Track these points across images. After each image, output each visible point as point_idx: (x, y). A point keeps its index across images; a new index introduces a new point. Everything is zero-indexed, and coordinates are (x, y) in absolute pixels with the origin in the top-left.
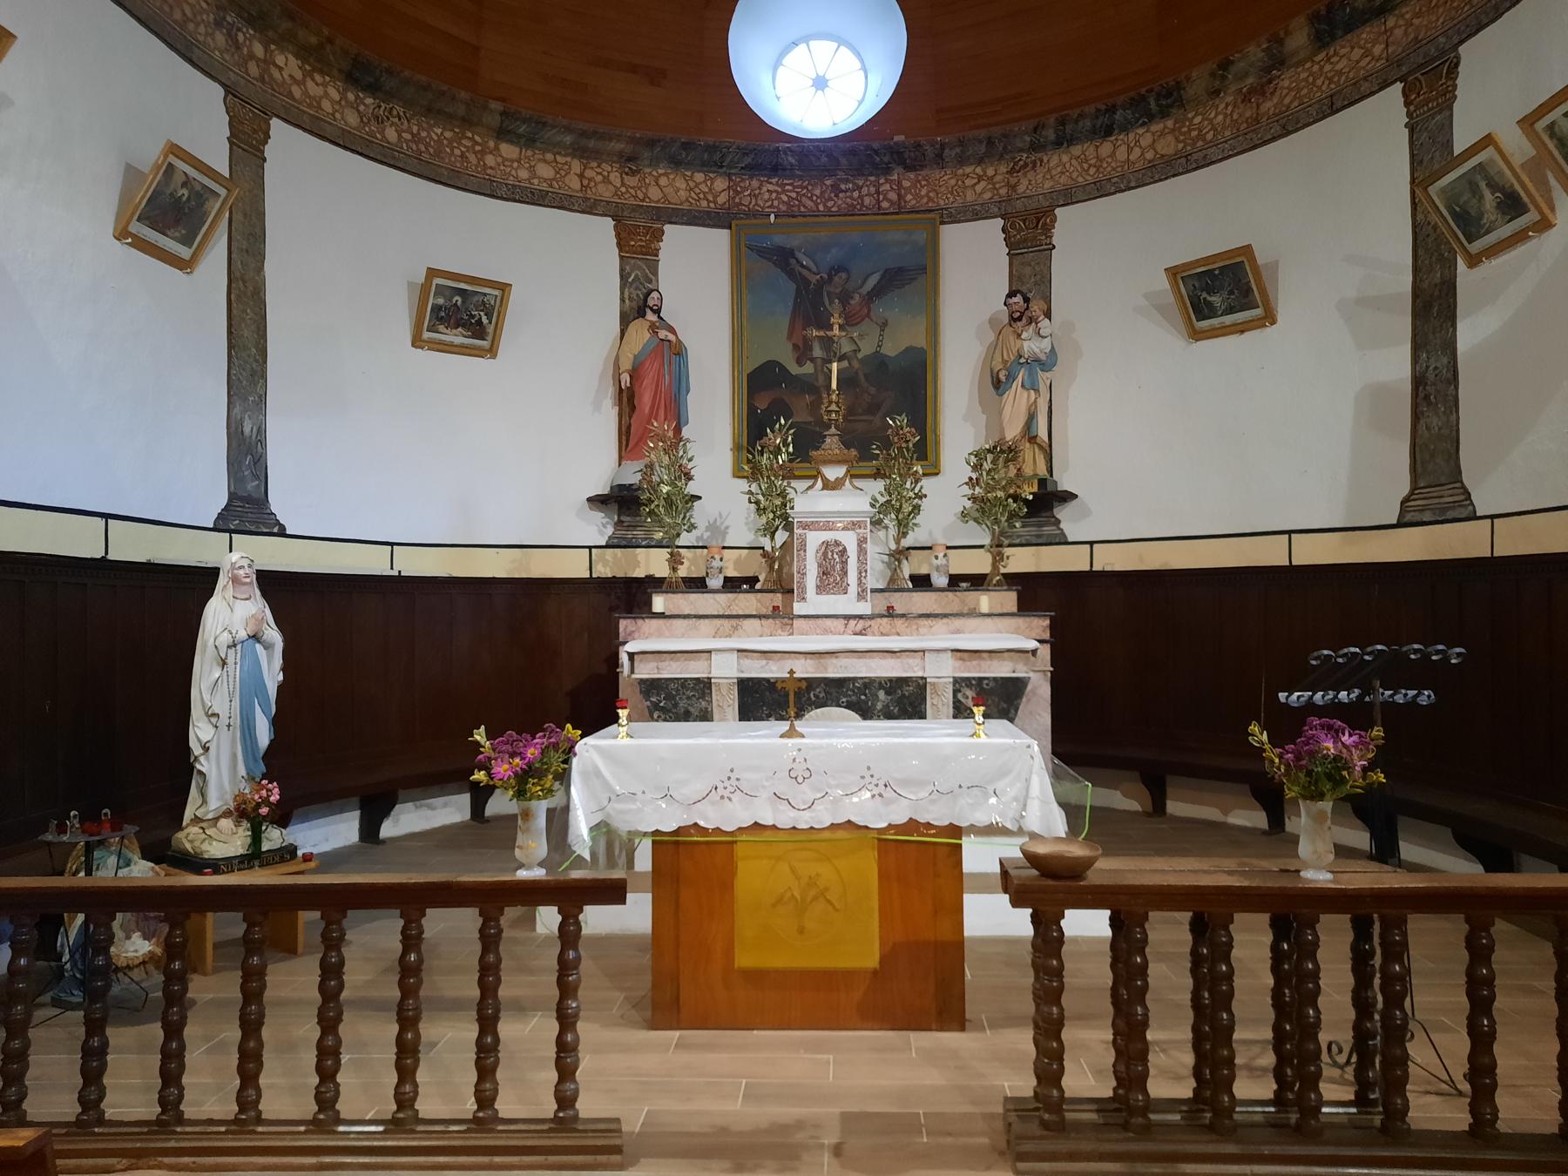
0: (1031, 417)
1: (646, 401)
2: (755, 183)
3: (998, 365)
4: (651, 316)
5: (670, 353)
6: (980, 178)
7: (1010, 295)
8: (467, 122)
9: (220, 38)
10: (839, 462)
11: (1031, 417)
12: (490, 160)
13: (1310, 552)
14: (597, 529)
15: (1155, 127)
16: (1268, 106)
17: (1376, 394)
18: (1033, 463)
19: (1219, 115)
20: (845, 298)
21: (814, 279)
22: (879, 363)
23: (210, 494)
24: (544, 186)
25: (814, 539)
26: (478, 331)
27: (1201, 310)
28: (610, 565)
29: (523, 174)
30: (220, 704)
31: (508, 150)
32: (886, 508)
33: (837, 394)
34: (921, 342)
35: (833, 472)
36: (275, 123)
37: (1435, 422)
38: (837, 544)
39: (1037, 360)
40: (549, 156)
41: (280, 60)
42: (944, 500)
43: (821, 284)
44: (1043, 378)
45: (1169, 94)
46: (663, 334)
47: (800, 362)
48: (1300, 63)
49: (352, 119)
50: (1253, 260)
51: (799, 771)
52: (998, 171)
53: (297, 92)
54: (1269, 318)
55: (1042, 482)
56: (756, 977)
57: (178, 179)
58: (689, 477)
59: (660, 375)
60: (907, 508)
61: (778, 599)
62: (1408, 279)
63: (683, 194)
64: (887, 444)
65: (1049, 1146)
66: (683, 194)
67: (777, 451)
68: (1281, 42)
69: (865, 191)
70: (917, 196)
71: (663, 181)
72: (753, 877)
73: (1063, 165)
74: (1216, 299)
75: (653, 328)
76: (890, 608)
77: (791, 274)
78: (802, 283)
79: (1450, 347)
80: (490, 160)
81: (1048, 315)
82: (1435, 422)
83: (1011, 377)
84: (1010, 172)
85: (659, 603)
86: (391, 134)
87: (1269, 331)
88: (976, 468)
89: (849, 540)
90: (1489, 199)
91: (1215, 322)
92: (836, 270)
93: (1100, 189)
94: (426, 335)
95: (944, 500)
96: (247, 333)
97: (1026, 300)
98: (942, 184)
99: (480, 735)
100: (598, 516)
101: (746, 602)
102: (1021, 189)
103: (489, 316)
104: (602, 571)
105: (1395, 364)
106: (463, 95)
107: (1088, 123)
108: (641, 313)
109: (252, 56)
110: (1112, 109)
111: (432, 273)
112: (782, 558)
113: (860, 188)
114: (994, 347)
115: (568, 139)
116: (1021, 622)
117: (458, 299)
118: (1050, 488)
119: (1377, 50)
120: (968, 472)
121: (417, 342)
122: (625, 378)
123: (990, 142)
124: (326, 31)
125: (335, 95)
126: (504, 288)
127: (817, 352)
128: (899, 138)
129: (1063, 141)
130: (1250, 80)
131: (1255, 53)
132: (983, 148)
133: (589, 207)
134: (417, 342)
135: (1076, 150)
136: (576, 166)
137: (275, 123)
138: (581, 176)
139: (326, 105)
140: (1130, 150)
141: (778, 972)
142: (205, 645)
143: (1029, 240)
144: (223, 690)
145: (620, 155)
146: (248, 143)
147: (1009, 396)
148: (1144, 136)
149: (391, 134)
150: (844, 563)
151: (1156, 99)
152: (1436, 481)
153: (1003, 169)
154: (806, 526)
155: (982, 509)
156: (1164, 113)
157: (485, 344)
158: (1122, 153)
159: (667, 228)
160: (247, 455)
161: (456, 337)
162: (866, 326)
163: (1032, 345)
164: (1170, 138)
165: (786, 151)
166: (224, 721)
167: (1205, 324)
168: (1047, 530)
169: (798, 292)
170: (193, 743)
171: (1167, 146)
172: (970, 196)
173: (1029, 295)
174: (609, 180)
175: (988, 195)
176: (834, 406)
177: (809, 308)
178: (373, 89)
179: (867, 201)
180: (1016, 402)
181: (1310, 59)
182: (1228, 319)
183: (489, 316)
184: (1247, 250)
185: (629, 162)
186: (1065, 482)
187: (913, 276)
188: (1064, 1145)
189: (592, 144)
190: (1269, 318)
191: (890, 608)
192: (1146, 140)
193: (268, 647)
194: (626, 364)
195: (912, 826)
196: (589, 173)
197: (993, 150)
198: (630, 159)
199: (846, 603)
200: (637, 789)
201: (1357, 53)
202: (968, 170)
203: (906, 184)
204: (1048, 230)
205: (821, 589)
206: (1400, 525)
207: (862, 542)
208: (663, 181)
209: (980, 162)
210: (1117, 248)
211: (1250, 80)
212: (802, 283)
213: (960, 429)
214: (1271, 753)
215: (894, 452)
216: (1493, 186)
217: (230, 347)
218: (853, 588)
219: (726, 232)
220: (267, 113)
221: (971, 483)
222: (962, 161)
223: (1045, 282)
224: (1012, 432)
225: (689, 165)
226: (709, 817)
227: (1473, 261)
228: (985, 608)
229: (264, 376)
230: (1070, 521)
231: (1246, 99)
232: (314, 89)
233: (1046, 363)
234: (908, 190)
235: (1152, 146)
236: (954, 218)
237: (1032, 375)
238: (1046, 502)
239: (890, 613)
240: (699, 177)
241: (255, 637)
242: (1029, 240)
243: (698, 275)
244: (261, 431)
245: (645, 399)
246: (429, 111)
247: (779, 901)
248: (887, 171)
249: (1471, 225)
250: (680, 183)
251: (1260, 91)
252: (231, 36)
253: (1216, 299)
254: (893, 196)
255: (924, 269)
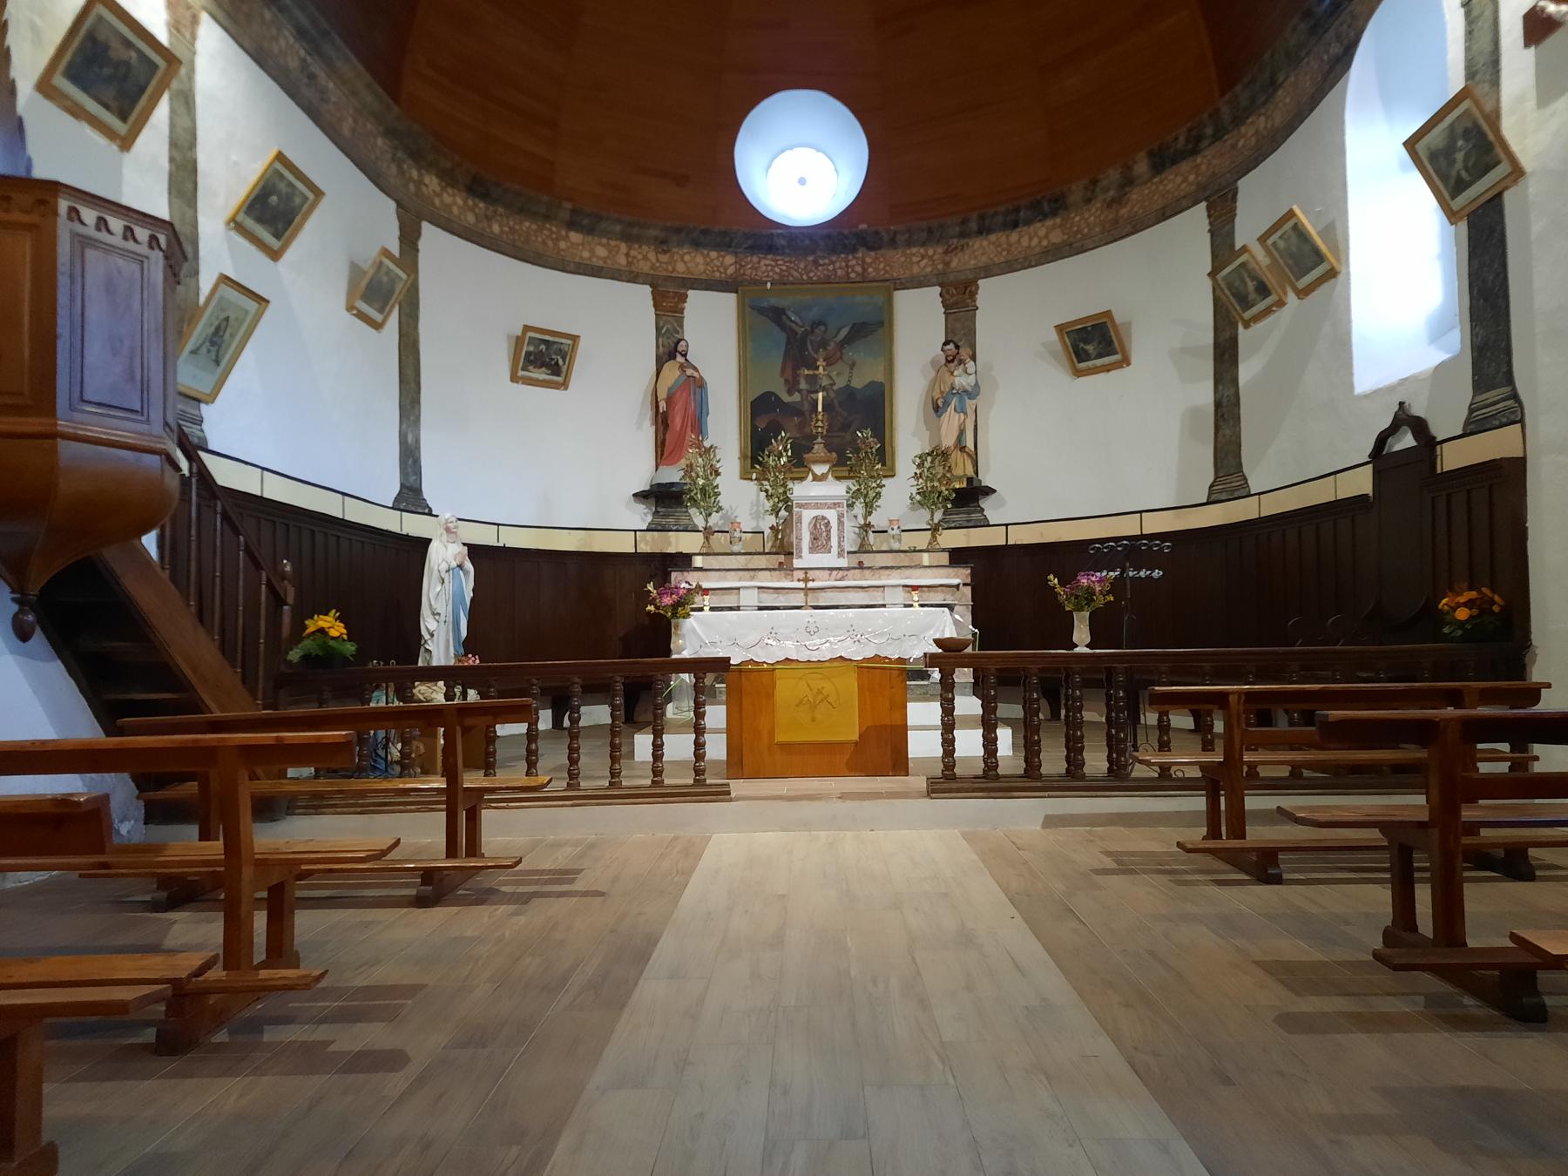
0: (962, 432)
1: (675, 421)
2: (755, 259)
3: (937, 395)
4: (680, 359)
5: (695, 385)
6: (923, 257)
7: (946, 344)
8: (547, 218)
9: (394, 169)
10: (824, 462)
11: (962, 432)
12: (563, 245)
13: (1155, 524)
14: (640, 516)
15: (1049, 223)
16: (1123, 211)
17: (1194, 413)
18: (962, 467)
19: (1090, 217)
20: (824, 344)
21: (800, 331)
22: (849, 392)
23: (390, 489)
24: (601, 263)
25: (808, 515)
26: (556, 370)
27: (1081, 356)
28: (649, 544)
29: (586, 254)
30: (440, 607)
31: (575, 237)
32: (856, 495)
33: (817, 413)
34: (880, 378)
35: (820, 469)
36: (425, 226)
37: (1228, 432)
38: (824, 518)
39: (965, 391)
40: (604, 241)
41: (427, 180)
42: (898, 495)
43: (806, 334)
44: (970, 404)
45: (1056, 201)
46: (689, 372)
47: (790, 393)
48: (1145, 183)
49: (471, 218)
50: (1113, 320)
51: (812, 628)
52: (935, 251)
53: (437, 201)
54: (1126, 361)
55: (970, 480)
56: (787, 747)
57: (384, 269)
58: (718, 474)
59: (687, 403)
60: (872, 494)
61: (782, 558)
62: (1211, 335)
63: (701, 268)
64: (857, 451)
65: (946, 786)
66: (701, 268)
67: (780, 456)
68: (1130, 168)
69: (837, 265)
70: (877, 270)
71: (687, 258)
72: (785, 690)
73: (983, 249)
74: (1090, 348)
75: (682, 367)
76: (861, 563)
77: (783, 327)
78: (791, 334)
79: (1235, 381)
80: (563, 245)
81: (973, 358)
82: (1228, 432)
83: (947, 404)
84: (946, 252)
85: (698, 561)
86: (496, 228)
87: (1126, 370)
88: (919, 466)
89: (831, 515)
90: (1251, 285)
91: (1090, 364)
92: (816, 324)
93: (1010, 267)
94: (521, 373)
95: (898, 495)
96: (410, 372)
97: (957, 347)
98: (896, 261)
99: (650, 587)
100: (641, 508)
101: (761, 561)
102: (953, 265)
103: (564, 359)
104: (644, 548)
105: (1204, 394)
106: (545, 198)
107: (1000, 218)
108: (672, 355)
109: (411, 179)
110: (1017, 210)
111: (527, 328)
112: (783, 531)
113: (833, 263)
114: (933, 382)
115: (618, 228)
116: (951, 570)
117: (543, 347)
118: (975, 484)
119: (1192, 178)
120: (914, 469)
121: (514, 378)
122: (663, 405)
123: (930, 231)
124: (457, 158)
125: (460, 201)
126: (575, 338)
127: (803, 385)
128: (863, 226)
129: (983, 231)
130: (1111, 193)
131: (1114, 175)
132: (925, 235)
133: (634, 278)
134: (514, 378)
135: (993, 237)
136: (623, 247)
137: (425, 226)
138: (627, 255)
139: (455, 210)
140: (1031, 239)
141: (800, 744)
142: (431, 571)
143: (959, 303)
144: (443, 598)
145: (656, 239)
146: (410, 238)
147: (945, 417)
148: (1040, 229)
149: (496, 228)
150: (829, 531)
151: (1051, 204)
152: (1228, 473)
153: (940, 250)
154: (801, 506)
155: (926, 498)
156: (1054, 214)
157: (560, 379)
158: (1025, 241)
159: (690, 293)
160: (410, 458)
161: (541, 374)
162: (839, 366)
163: (962, 380)
164: (1058, 231)
165: (779, 235)
166: (442, 618)
167: (1083, 365)
168: (975, 516)
169: (788, 342)
170: (424, 632)
171: (1057, 237)
172: (916, 270)
173: (959, 341)
174: (647, 258)
175: (929, 269)
176: (820, 424)
177: (798, 354)
178: (485, 197)
179: (839, 272)
180: (950, 423)
181: (1150, 180)
182: (1099, 362)
183: (564, 359)
184: (1108, 314)
185: (662, 244)
186: (987, 480)
187: (874, 329)
188: (954, 785)
189: (635, 231)
190: (1126, 361)
191: (861, 563)
192: (1042, 233)
193: (466, 573)
194: (662, 395)
195: (877, 658)
196: (633, 253)
197: (932, 236)
198: (664, 242)
199: (831, 559)
200: (717, 638)
201: (1179, 179)
202: (914, 250)
203: (868, 260)
204: (973, 295)
205: (813, 550)
206: (1207, 503)
207: (840, 516)
208: (687, 258)
209: (923, 244)
210: (1022, 309)
211: (1111, 193)
212: (791, 334)
213: (909, 438)
214: (1059, 589)
215: (862, 455)
216: (1253, 278)
217: (401, 382)
218: (835, 549)
219: (733, 296)
220: (420, 218)
221: (917, 477)
222: (909, 244)
223: (971, 334)
224: (948, 441)
225: (705, 246)
226: (760, 656)
227: (1247, 325)
228: (926, 563)
229: (419, 402)
230: (991, 509)
231: (1109, 205)
232: (447, 199)
233: (972, 393)
234: (870, 265)
235: (1046, 236)
236: (904, 285)
237: (962, 401)
238: (969, 498)
239: (861, 566)
240: (713, 254)
241: (460, 566)
242: (959, 303)
243: (712, 324)
244: (417, 441)
245: (677, 422)
246: (521, 211)
247: (800, 703)
248: (854, 250)
249: (1246, 303)
250: (700, 259)
251: (1117, 201)
252: (399, 167)
253: (1090, 348)
254: (859, 269)
255: (883, 323)
